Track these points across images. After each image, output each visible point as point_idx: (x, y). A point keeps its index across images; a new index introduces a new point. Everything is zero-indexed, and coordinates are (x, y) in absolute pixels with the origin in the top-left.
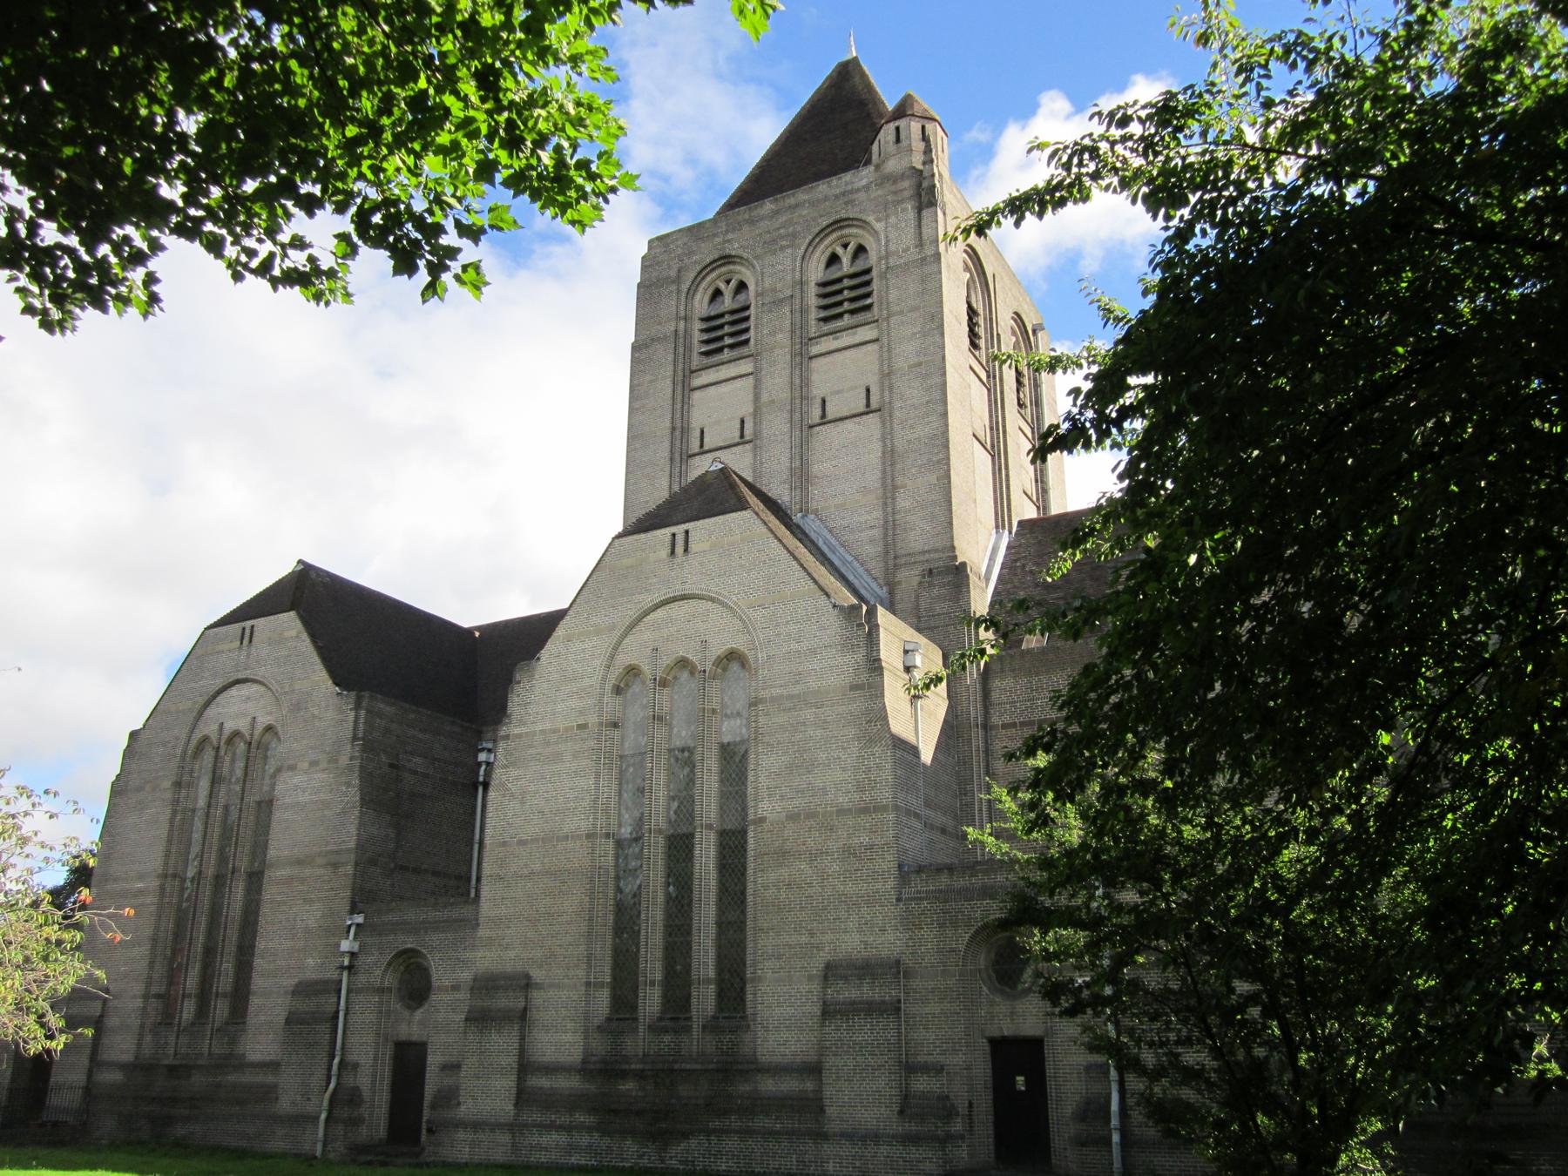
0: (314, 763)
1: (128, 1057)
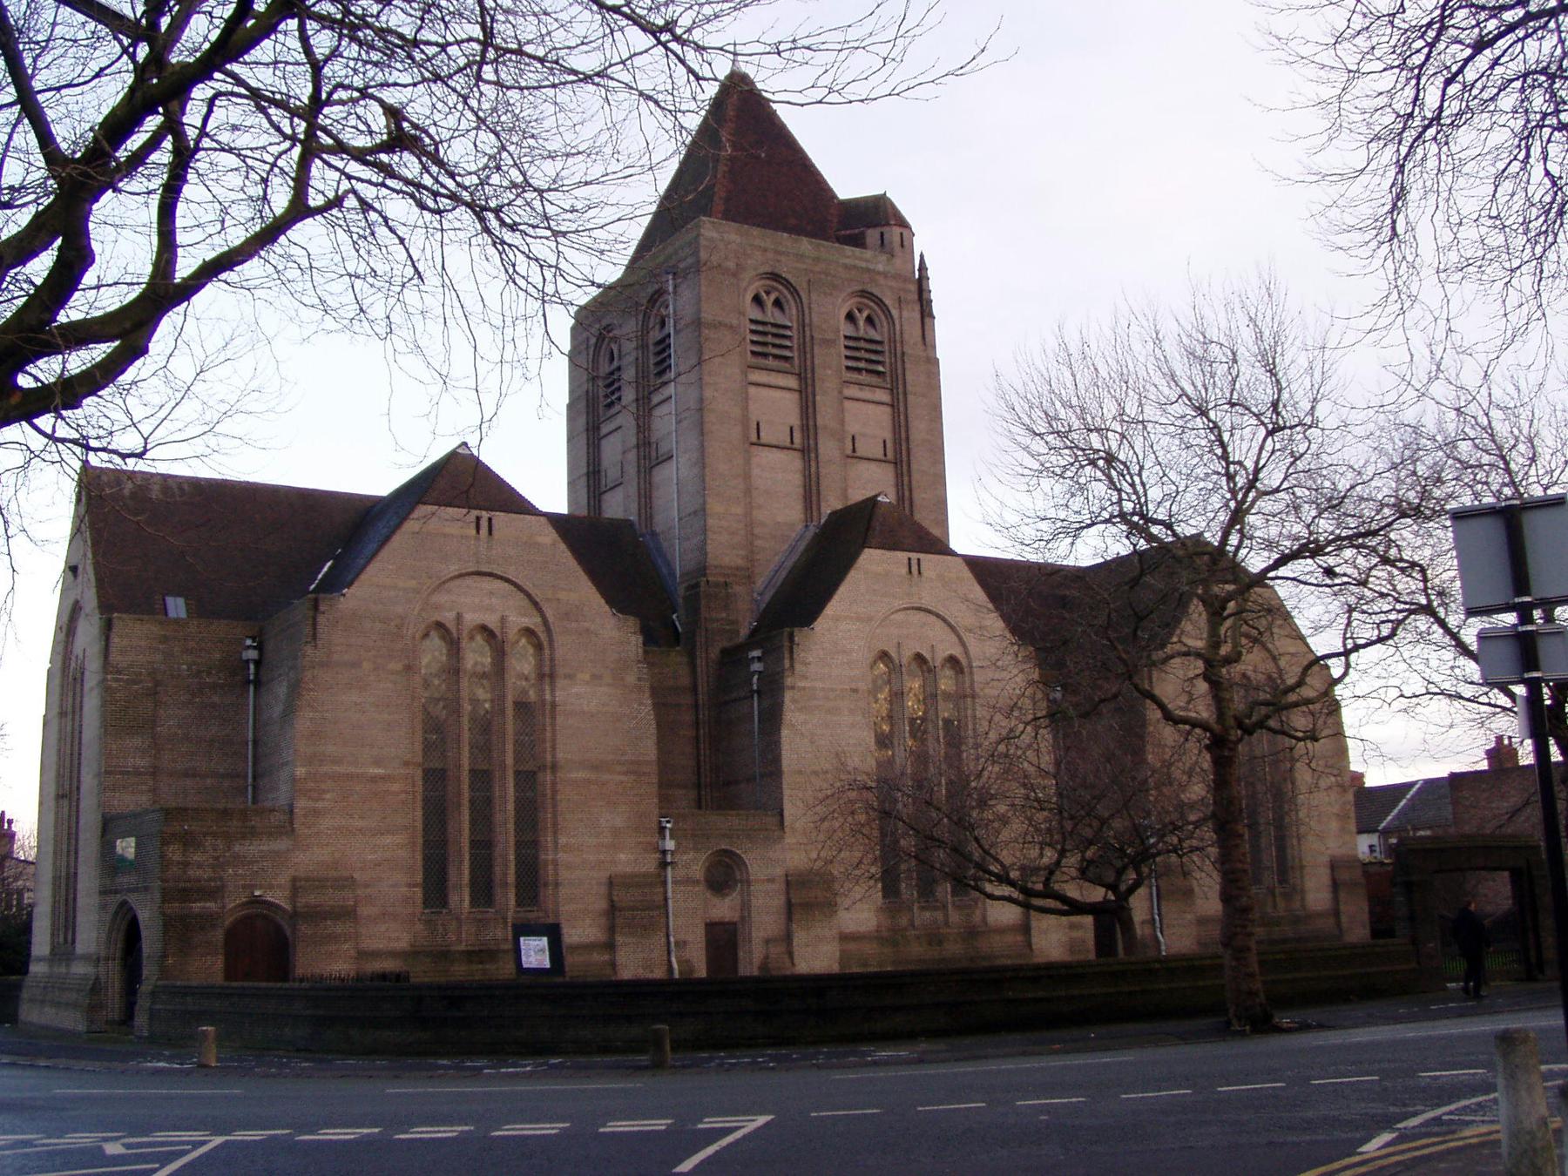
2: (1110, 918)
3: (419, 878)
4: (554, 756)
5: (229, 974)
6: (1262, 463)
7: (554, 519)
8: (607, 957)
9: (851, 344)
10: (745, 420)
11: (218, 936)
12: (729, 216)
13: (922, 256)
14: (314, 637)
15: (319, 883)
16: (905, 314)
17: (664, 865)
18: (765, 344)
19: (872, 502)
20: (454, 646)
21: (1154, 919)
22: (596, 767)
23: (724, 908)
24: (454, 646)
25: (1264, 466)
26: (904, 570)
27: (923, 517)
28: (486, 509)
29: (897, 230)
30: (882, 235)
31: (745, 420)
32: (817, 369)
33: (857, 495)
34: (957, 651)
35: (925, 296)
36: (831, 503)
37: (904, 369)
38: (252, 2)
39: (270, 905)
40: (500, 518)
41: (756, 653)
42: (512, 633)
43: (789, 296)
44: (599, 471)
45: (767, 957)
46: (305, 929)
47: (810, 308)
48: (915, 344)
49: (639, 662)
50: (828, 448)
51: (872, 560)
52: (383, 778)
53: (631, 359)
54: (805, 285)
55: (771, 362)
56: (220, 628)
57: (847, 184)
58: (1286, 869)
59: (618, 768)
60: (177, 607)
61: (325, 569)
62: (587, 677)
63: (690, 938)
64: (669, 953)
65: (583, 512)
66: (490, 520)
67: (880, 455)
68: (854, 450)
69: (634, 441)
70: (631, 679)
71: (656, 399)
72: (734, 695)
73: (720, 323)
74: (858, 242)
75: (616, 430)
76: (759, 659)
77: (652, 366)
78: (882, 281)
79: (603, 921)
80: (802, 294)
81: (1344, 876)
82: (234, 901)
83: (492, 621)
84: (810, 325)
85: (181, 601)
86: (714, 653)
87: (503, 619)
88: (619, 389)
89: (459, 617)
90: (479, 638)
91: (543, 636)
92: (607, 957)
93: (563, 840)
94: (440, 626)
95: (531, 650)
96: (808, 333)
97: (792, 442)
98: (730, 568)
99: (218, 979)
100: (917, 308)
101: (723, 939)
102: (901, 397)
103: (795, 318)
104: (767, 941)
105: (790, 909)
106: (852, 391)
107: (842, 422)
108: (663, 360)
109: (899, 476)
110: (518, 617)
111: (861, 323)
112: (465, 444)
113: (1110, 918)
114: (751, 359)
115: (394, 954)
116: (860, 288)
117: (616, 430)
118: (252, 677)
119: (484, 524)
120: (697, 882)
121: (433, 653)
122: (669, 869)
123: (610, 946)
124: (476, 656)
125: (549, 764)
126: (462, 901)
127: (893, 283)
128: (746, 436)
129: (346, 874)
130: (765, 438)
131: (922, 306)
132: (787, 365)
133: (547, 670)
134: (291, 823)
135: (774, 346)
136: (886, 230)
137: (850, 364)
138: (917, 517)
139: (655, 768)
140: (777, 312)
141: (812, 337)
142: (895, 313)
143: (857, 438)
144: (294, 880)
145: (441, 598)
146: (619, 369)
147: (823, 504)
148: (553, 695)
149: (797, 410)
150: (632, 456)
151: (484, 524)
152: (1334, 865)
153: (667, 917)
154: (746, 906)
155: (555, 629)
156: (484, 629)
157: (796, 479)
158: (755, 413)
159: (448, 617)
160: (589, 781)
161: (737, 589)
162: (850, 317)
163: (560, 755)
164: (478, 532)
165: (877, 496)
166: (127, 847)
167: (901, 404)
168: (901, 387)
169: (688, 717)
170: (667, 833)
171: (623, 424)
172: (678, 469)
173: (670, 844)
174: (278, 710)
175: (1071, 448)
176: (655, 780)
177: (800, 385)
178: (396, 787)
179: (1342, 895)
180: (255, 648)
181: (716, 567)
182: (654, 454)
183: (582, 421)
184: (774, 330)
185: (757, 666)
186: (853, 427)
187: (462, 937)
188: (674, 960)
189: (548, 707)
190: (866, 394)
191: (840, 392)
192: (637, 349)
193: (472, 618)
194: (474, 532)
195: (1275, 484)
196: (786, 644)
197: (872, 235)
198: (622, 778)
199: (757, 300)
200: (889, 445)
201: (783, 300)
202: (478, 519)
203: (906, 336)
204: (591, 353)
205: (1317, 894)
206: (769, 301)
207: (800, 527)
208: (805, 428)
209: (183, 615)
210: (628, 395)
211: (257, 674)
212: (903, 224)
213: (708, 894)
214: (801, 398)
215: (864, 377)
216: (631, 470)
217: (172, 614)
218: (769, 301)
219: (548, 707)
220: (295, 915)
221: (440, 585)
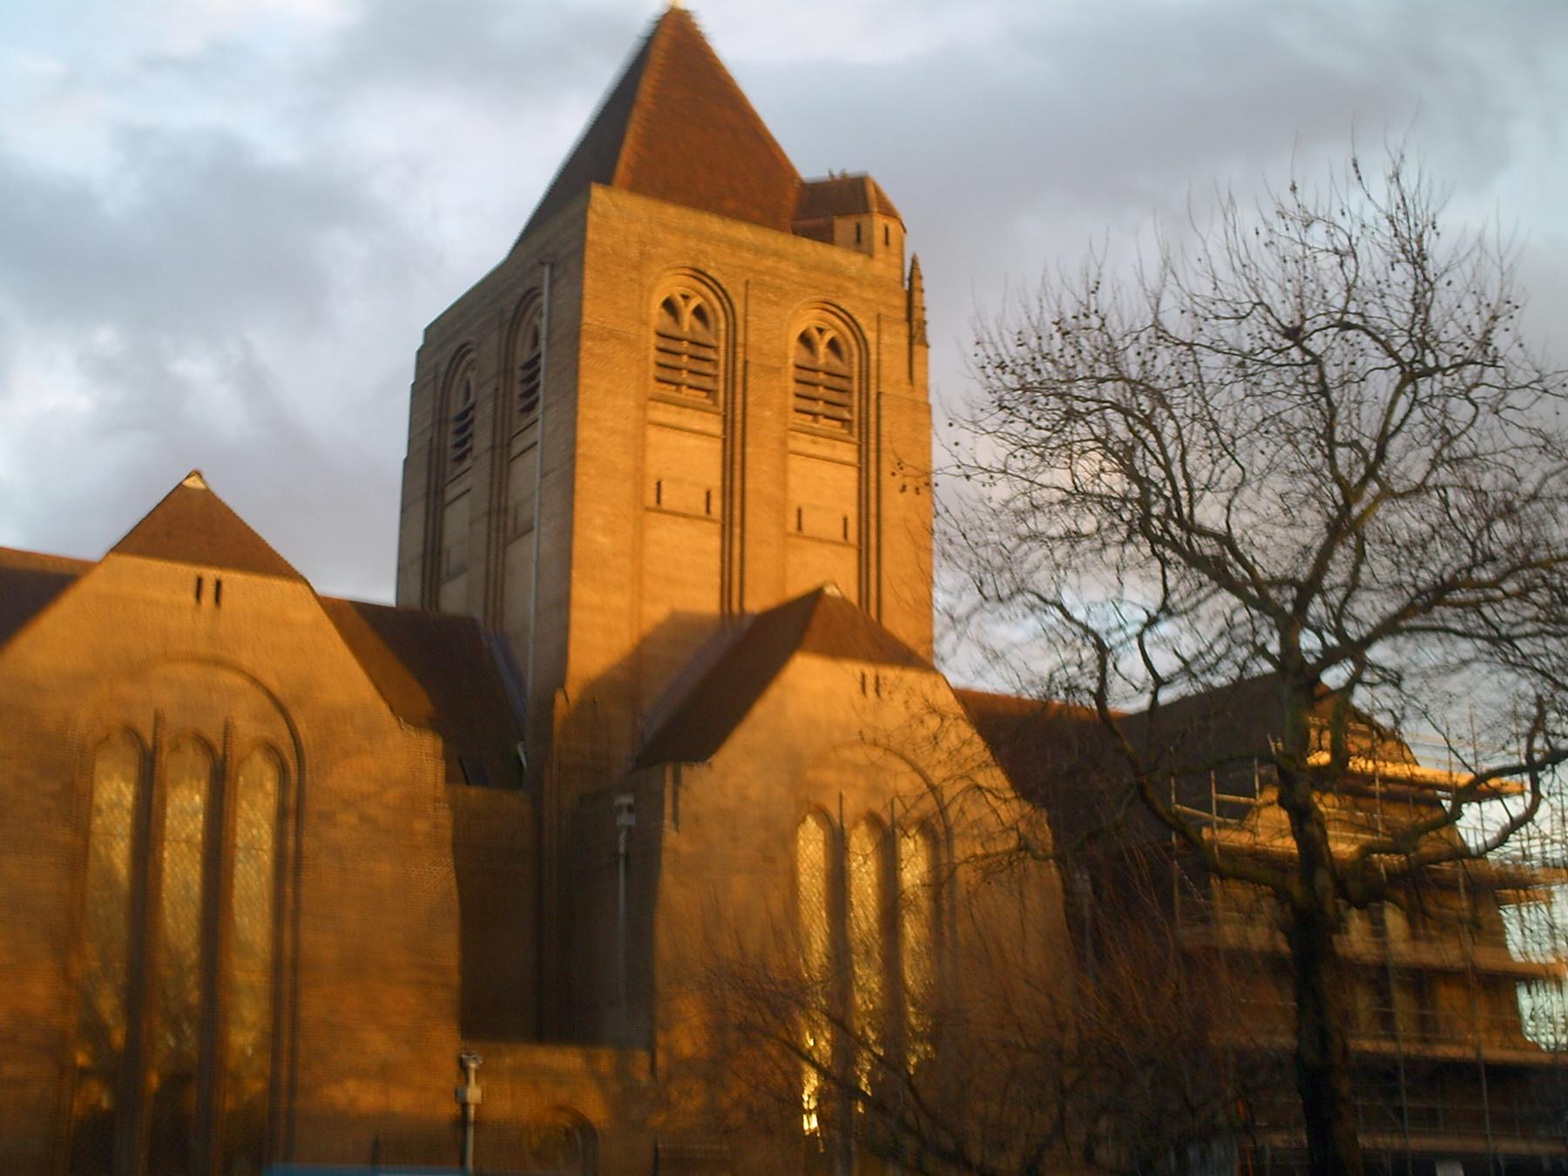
6: (1396, 419)
9: (806, 375)
10: (638, 476)
12: (639, 186)
13: (914, 262)
16: (886, 339)
25: (1398, 429)
27: (899, 625)
28: (210, 563)
29: (879, 222)
30: (858, 228)
31: (638, 476)
32: (750, 409)
33: (798, 586)
35: (917, 314)
36: (758, 600)
37: (878, 417)
38: (1465, 1174)
40: (234, 580)
43: (717, 304)
47: (746, 321)
48: (898, 382)
50: (760, 522)
53: (490, 389)
54: (741, 289)
65: (414, 601)
66: (218, 584)
67: (839, 536)
68: (800, 527)
69: (485, 506)
71: (518, 446)
74: (824, 235)
75: (465, 493)
77: (516, 398)
78: (853, 288)
80: (735, 300)
84: (745, 345)
88: (471, 435)
91: (292, 765)
96: (740, 356)
97: (708, 511)
100: (903, 330)
102: (873, 456)
103: (722, 335)
107: (784, 486)
111: (822, 348)
112: (198, 474)
114: (655, 388)
116: (822, 297)
117: (465, 493)
119: (209, 590)
127: (869, 295)
128: (639, 497)
130: (665, 504)
131: (911, 328)
132: (709, 402)
136: (864, 220)
138: (887, 623)
140: (698, 326)
141: (746, 363)
142: (871, 336)
143: (805, 511)
146: (472, 407)
151: (209, 590)
158: (656, 465)
168: (873, 441)
171: (473, 480)
172: (538, 543)
182: (511, 523)
183: (422, 480)
185: (624, 820)
190: (823, 449)
191: (784, 443)
192: (498, 374)
194: (191, 598)
195: (1417, 477)
199: (669, 305)
200: (853, 523)
201: (707, 308)
202: (200, 581)
203: (885, 371)
204: (440, 384)
208: (727, 493)
210: (482, 441)
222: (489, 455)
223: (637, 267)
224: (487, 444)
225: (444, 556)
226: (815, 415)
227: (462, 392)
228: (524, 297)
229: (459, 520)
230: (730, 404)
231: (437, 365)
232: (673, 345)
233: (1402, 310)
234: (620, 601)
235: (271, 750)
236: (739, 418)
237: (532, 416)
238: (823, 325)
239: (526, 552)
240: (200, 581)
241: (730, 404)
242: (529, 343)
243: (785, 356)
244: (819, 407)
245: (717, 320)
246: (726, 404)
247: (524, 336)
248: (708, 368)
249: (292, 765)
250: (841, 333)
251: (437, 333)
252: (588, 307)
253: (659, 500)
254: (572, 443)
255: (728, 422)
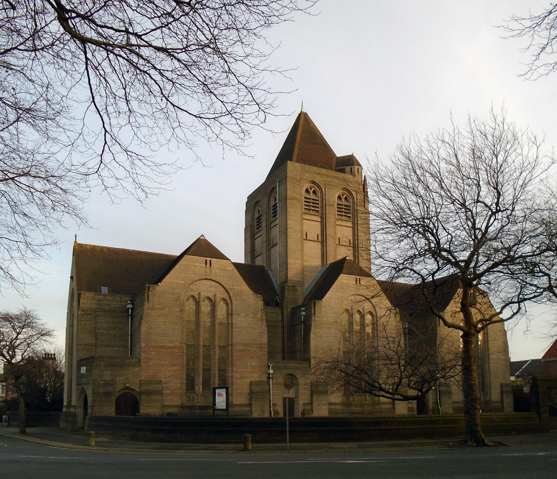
0: (247, 315)
1: (178, 403)
2: (421, 401)
3: (185, 381)
4: (232, 341)
5: (118, 411)
7: (237, 265)
8: (249, 409)
11: (114, 398)
12: (297, 161)
13: (365, 177)
14: (148, 300)
15: (149, 383)
17: (269, 378)
18: (309, 206)
19: (344, 259)
20: (198, 304)
21: (437, 401)
22: (246, 345)
23: (291, 394)
24: (198, 304)
26: (354, 283)
27: (363, 264)
29: (356, 167)
33: (339, 258)
34: (372, 310)
35: (366, 190)
36: (331, 260)
39: (133, 389)
40: (214, 260)
41: (303, 309)
42: (218, 300)
43: (318, 189)
44: (255, 250)
45: (304, 410)
46: (143, 397)
49: (262, 310)
50: (330, 241)
51: (343, 279)
52: (172, 347)
55: (311, 212)
56: (118, 297)
57: (340, 151)
58: (484, 386)
59: (254, 346)
60: (105, 290)
61: (525, 366)
62: (244, 315)
63: (277, 403)
64: (270, 407)
66: (210, 261)
68: (339, 243)
69: (265, 240)
70: (259, 316)
72: (296, 323)
73: (294, 198)
74: (343, 171)
76: (304, 311)
79: (248, 397)
81: (505, 389)
82: (119, 387)
83: (211, 295)
85: (106, 288)
86: (289, 310)
87: (215, 295)
89: (199, 294)
90: (206, 301)
91: (229, 301)
92: (249, 409)
93: (235, 369)
94: (193, 296)
95: (225, 306)
96: (324, 202)
97: (318, 239)
98: (295, 281)
99: (113, 414)
101: (290, 403)
104: (304, 404)
105: (312, 394)
106: (339, 222)
108: (275, 212)
109: (354, 251)
110: (221, 294)
112: (203, 235)
113: (421, 401)
115: (175, 406)
116: (343, 187)
118: (130, 314)
120: (280, 384)
121: (190, 306)
122: (271, 379)
123: (250, 405)
124: (205, 308)
125: (230, 344)
126: (199, 389)
128: (302, 237)
129: (158, 379)
130: (308, 239)
133: (230, 312)
134: (140, 362)
135: (313, 206)
136: (352, 167)
137: (338, 213)
139: (267, 346)
141: (326, 204)
144: (140, 381)
145: (194, 287)
146: (261, 216)
147: (328, 260)
148: (232, 320)
149: (320, 229)
150: (265, 244)
151: (208, 262)
152: (501, 386)
153: (270, 395)
154: (297, 393)
155: (233, 299)
156: (208, 298)
157: (319, 252)
159: (196, 294)
160: (244, 350)
161: (298, 288)
162: (339, 197)
163: (234, 341)
164: (206, 265)
165: (346, 257)
166: (83, 370)
167: (356, 227)
169: (280, 330)
170: (271, 367)
173: (271, 371)
174: (137, 325)
175: (435, 227)
176: (267, 350)
177: (321, 220)
178: (177, 351)
179: (504, 396)
180: (131, 304)
181: (291, 281)
184: (313, 201)
185: (303, 313)
186: (339, 235)
187: (200, 401)
188: (272, 409)
189: (230, 325)
190: (344, 223)
191: (335, 223)
193: (203, 294)
196: (313, 306)
197: (348, 169)
198: (256, 349)
200: (351, 241)
202: (206, 260)
205: (495, 395)
206: (311, 191)
207: (320, 268)
208: (322, 235)
209: (107, 292)
210: (264, 224)
211: (132, 313)
212: (359, 165)
213: (284, 388)
214: (321, 224)
215: (344, 218)
216: (265, 250)
217: (103, 292)
218: (311, 191)
219: (230, 325)
220: (140, 393)
221: (193, 283)
222: (265, 228)
223: (299, 182)
224: (265, 225)
225: (256, 251)
226: (342, 215)
227: (258, 212)
228: (272, 189)
229: (258, 242)
230: (322, 214)
231: (251, 206)
232: (308, 200)
233: (473, 180)
234: (299, 262)
235: (224, 299)
236: (324, 217)
237: (276, 218)
238: (343, 194)
239: (276, 251)
240: (206, 260)
241: (322, 214)
242: (274, 200)
243: (335, 202)
244: (343, 214)
245: (318, 193)
246: (321, 214)
247: (272, 199)
248: (317, 206)
249: (229, 301)
250: (348, 195)
251: (251, 198)
252: (288, 192)
253: (306, 237)
254: (286, 225)
255: (322, 218)
